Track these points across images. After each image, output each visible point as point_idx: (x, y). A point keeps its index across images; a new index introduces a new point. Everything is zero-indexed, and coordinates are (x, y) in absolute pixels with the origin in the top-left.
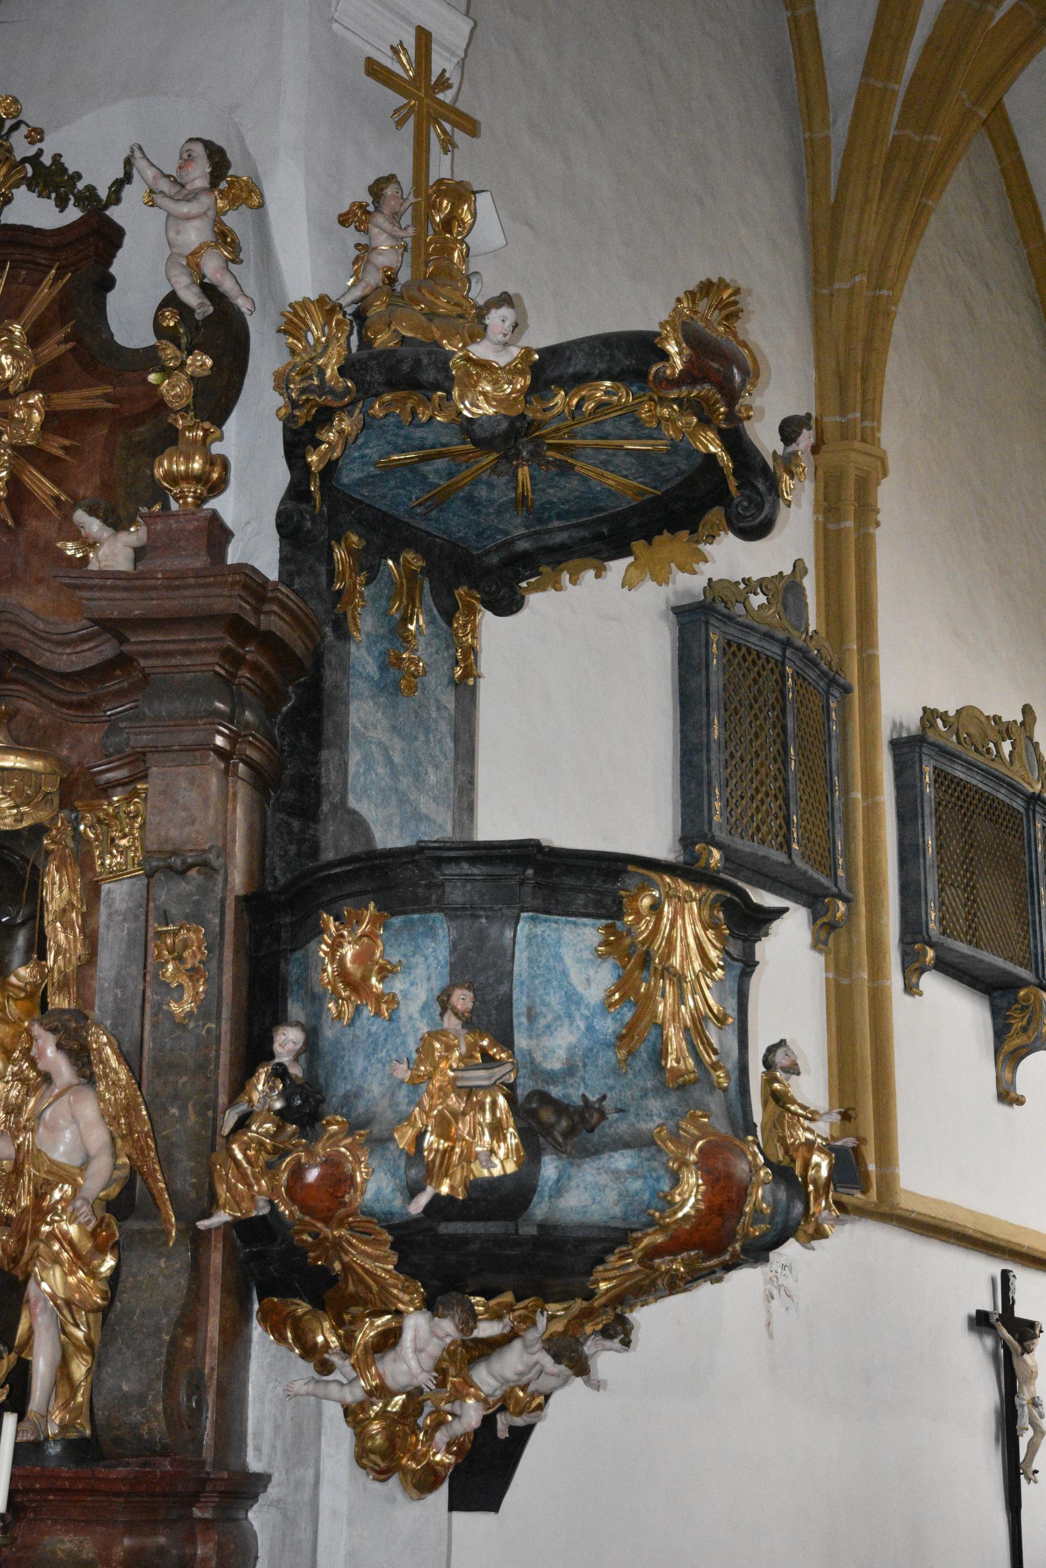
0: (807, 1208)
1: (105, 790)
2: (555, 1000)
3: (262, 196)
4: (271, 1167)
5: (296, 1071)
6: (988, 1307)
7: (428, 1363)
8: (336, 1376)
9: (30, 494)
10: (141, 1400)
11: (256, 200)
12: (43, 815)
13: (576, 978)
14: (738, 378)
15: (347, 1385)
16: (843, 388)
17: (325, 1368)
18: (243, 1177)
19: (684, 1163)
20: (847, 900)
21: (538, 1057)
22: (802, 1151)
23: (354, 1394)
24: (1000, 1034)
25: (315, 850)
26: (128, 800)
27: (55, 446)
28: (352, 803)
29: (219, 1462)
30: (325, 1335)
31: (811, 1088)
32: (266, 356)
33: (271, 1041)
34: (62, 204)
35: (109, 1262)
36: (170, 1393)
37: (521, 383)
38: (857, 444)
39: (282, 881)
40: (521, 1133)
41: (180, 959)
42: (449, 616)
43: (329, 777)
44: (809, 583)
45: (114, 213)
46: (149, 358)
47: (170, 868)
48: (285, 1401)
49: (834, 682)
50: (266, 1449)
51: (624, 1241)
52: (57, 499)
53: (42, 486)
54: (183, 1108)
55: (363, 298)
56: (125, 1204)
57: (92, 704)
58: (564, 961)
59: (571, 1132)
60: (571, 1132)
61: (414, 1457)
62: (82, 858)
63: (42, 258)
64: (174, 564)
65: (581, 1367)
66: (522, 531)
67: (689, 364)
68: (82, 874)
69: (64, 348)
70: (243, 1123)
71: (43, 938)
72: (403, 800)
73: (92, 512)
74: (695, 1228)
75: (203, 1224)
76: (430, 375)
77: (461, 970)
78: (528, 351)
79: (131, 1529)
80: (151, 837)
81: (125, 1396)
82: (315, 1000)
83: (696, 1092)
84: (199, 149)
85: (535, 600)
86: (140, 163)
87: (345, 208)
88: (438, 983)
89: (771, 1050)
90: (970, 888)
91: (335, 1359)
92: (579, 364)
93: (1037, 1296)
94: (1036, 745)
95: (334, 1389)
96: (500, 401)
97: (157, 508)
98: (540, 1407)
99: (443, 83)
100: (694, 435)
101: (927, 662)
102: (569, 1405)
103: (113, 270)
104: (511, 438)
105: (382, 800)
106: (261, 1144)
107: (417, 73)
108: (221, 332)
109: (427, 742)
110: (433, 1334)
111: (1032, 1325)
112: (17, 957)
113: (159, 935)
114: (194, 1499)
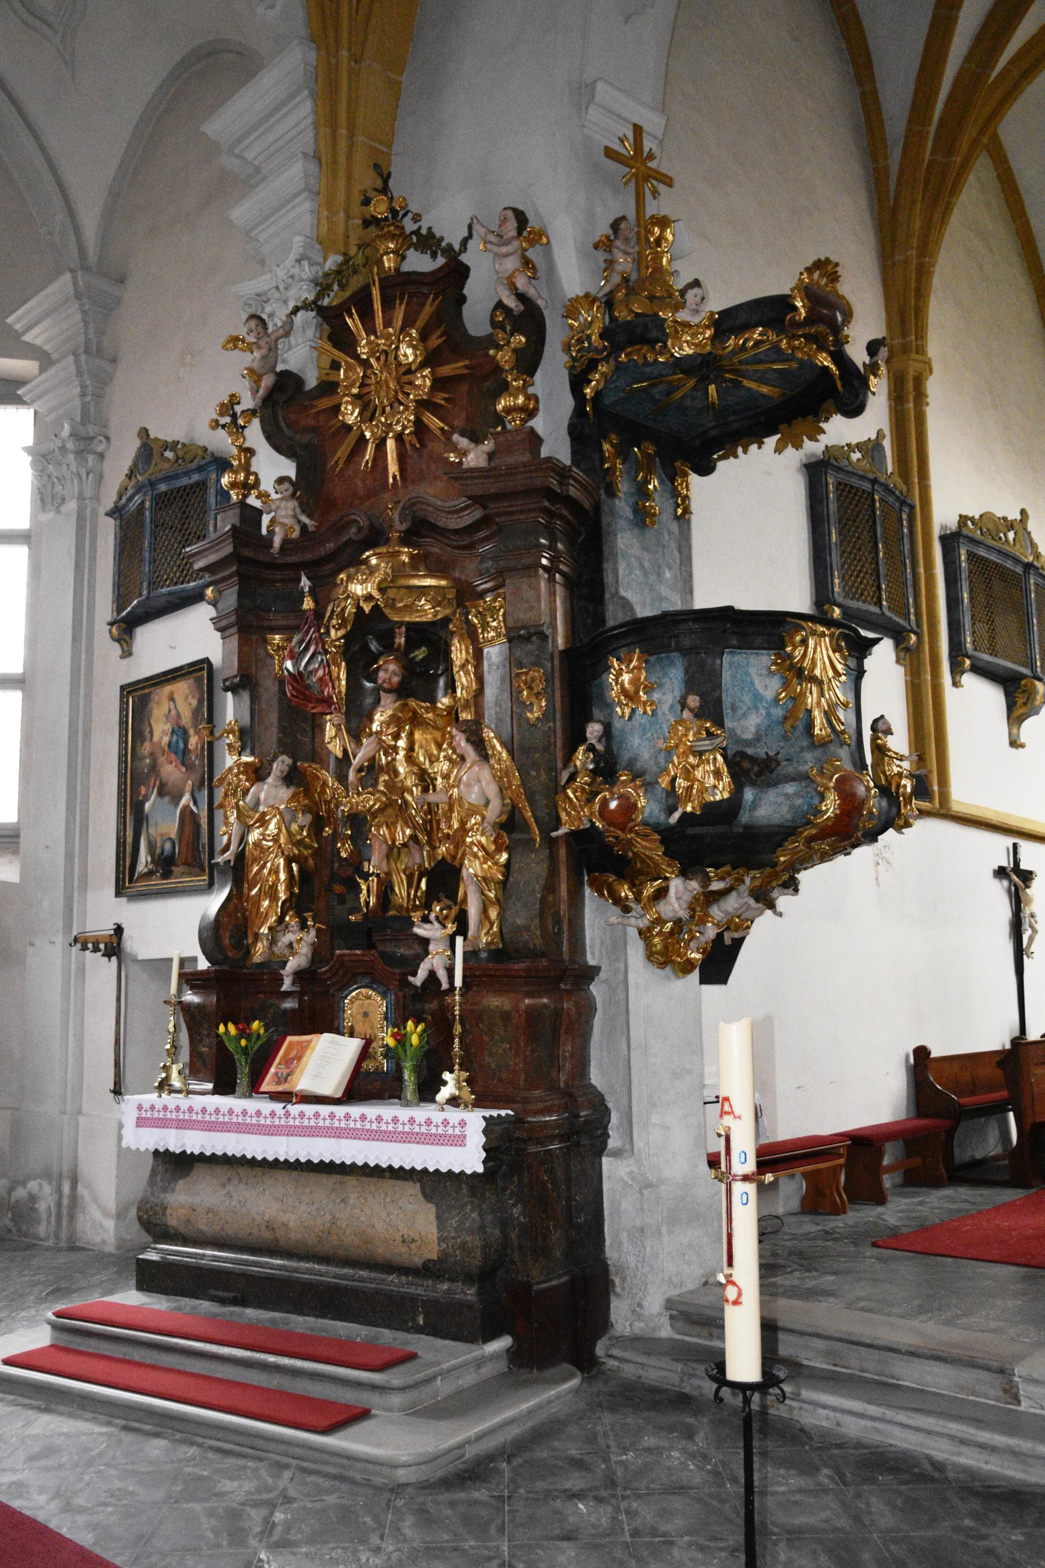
0: (899, 810)
1: (482, 595)
2: (747, 699)
3: (547, 237)
4: (590, 801)
5: (600, 747)
6: (1005, 864)
7: (684, 905)
8: (633, 913)
9: (427, 427)
10: (527, 928)
11: (545, 240)
12: (448, 611)
13: (759, 685)
14: (840, 318)
15: (638, 919)
16: (903, 322)
17: (627, 910)
18: (574, 808)
19: (827, 788)
20: (916, 633)
21: (738, 731)
22: (897, 778)
23: (643, 923)
24: (1011, 707)
25: (603, 621)
26: (495, 600)
27: (440, 399)
28: (622, 592)
29: (573, 961)
30: (625, 892)
31: (899, 742)
32: (555, 335)
33: (585, 732)
34: (434, 256)
35: (504, 856)
36: (543, 926)
37: (708, 333)
38: (913, 355)
39: (585, 641)
40: (732, 775)
41: (530, 688)
42: (672, 480)
43: (609, 578)
44: (887, 443)
45: (464, 258)
46: (490, 341)
47: (520, 636)
48: (603, 927)
49: (904, 502)
50: (597, 953)
51: (793, 834)
52: (442, 429)
53: (434, 422)
54: (538, 771)
55: (611, 292)
56: (510, 825)
57: (471, 546)
58: (751, 679)
59: (759, 774)
60: (759, 774)
61: (679, 956)
62: (471, 635)
63: (425, 290)
64: (511, 460)
65: (771, 906)
66: (713, 424)
67: (809, 312)
68: (473, 644)
69: (440, 341)
70: (572, 778)
71: (453, 681)
72: (652, 589)
73: (463, 435)
74: (834, 824)
75: (554, 834)
76: (654, 334)
77: (691, 685)
78: (712, 313)
79: (528, 995)
80: (509, 619)
81: (519, 927)
82: (609, 706)
83: (832, 747)
84: (510, 214)
85: (721, 465)
86: (476, 227)
87: (597, 239)
88: (677, 694)
89: (876, 721)
90: (991, 622)
91: (632, 904)
92: (742, 318)
93: (1031, 856)
94: (1029, 533)
95: (633, 921)
96: (696, 345)
97: (499, 429)
98: (748, 927)
99: (651, 156)
100: (816, 354)
101: (961, 487)
102: (764, 924)
103: (465, 292)
104: (704, 367)
105: (637, 588)
106: (583, 789)
107: (635, 151)
108: (528, 319)
109: (664, 555)
110: (686, 888)
111: (1031, 873)
112: (440, 693)
113: (518, 675)
114: (561, 979)
